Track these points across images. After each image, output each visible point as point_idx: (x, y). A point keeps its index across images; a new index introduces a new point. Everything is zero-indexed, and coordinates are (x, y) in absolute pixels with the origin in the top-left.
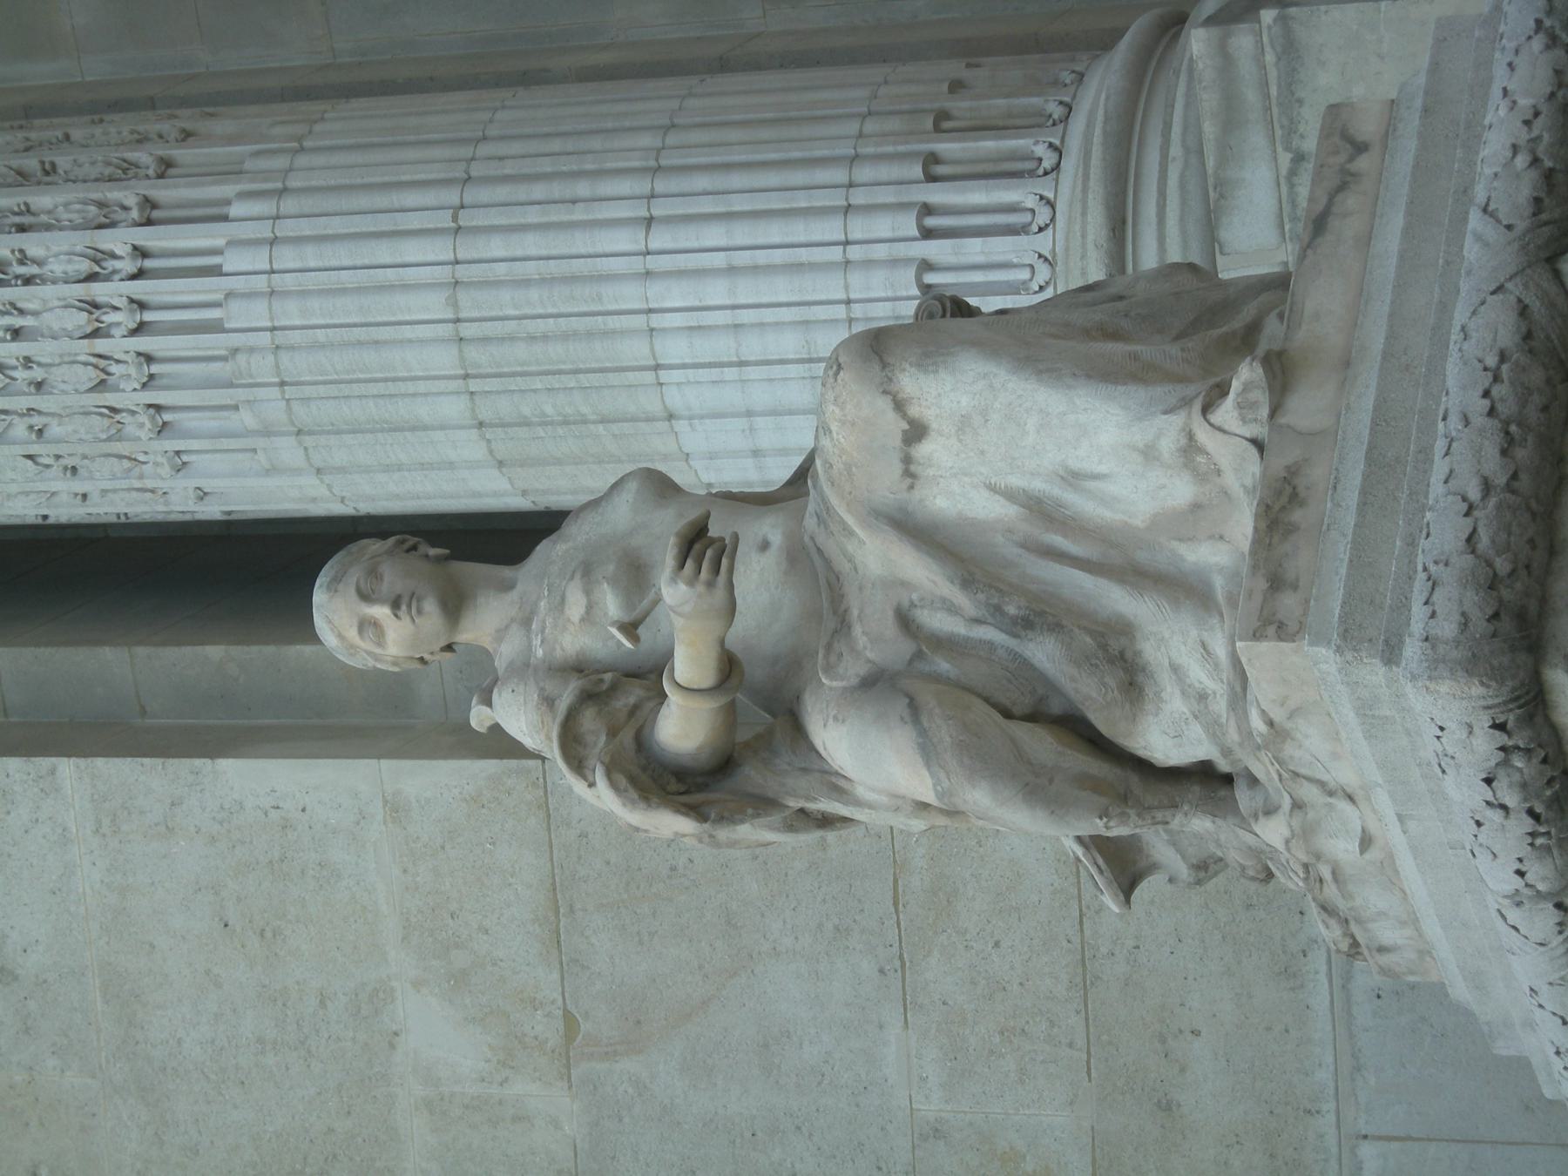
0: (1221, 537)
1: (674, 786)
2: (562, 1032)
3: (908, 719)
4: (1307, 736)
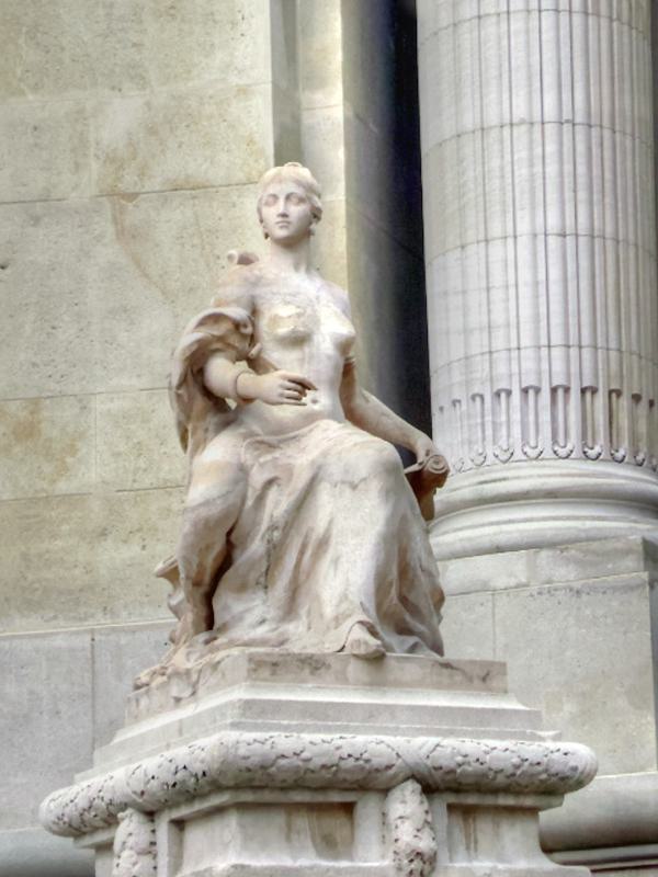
1: (195, 369)
2: (128, 191)
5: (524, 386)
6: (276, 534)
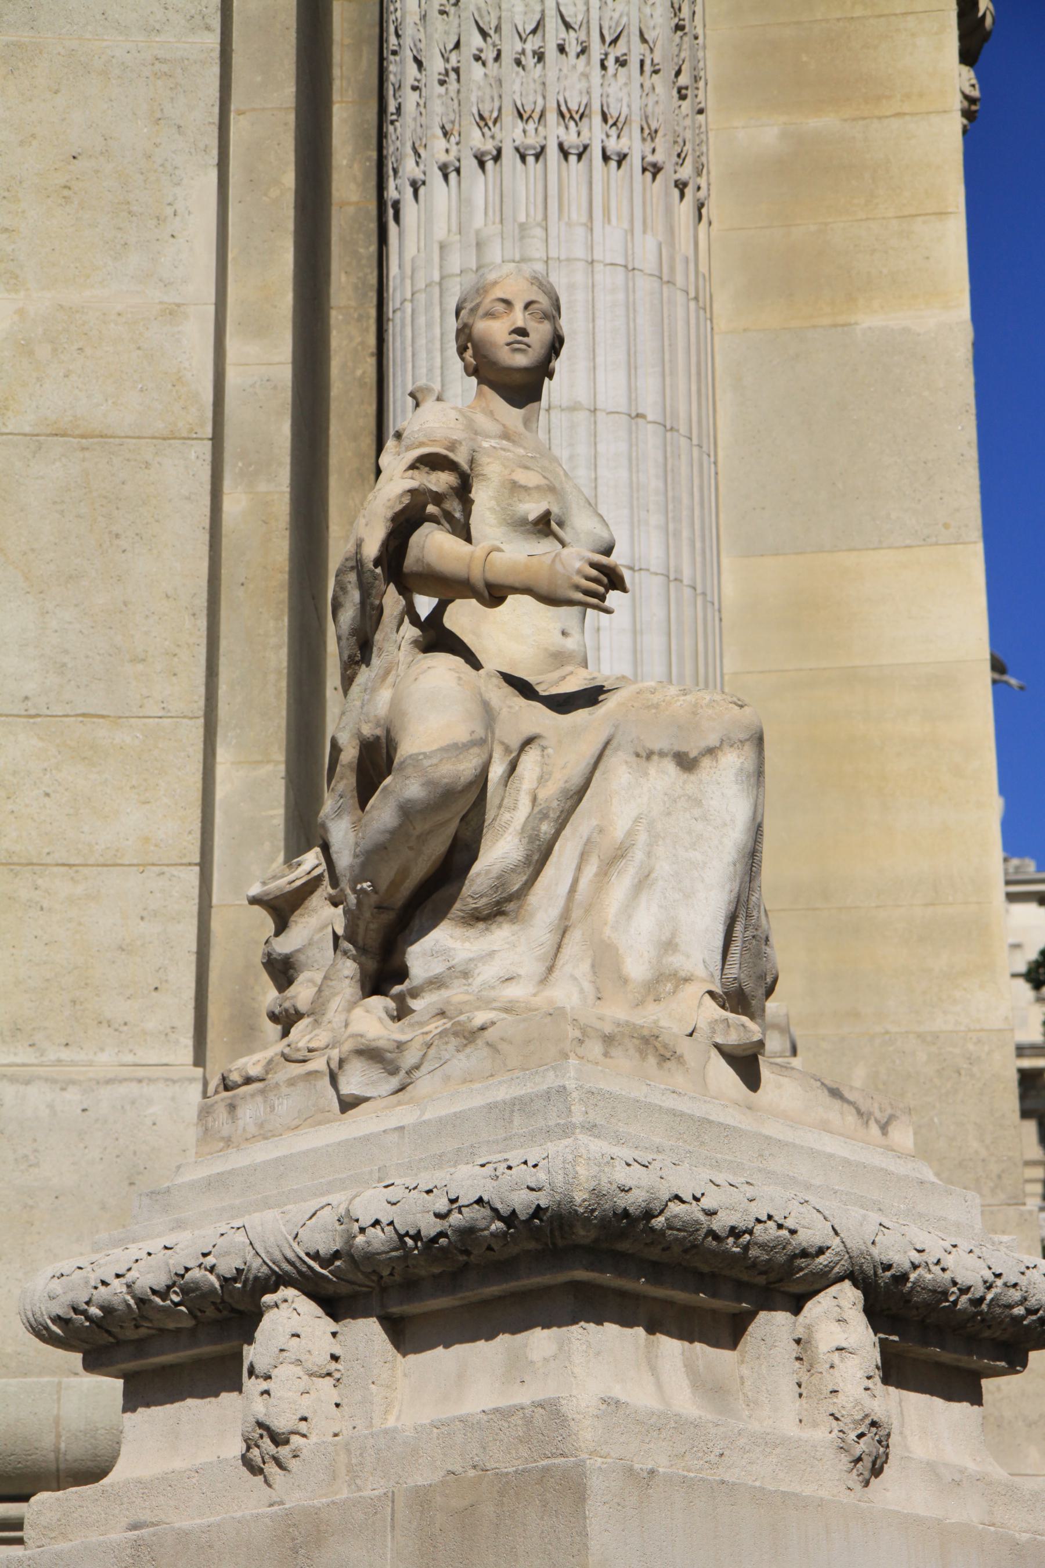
4: (468, 1057)
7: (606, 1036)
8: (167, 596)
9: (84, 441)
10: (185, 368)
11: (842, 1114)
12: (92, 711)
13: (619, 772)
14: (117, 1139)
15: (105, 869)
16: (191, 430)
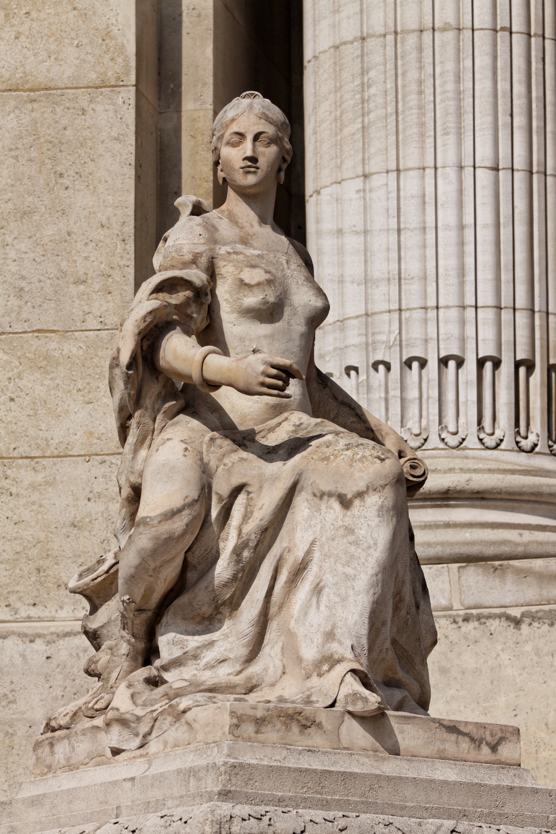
0: (284, 673)
3: (187, 501)
5: (443, 354)
6: (246, 554)
7: (258, 719)
8: (102, 226)
9: (32, 94)
10: (112, 24)
11: (457, 743)
12: (45, 328)
13: (302, 506)
14: (74, 680)
15: (59, 459)
16: (118, 79)
